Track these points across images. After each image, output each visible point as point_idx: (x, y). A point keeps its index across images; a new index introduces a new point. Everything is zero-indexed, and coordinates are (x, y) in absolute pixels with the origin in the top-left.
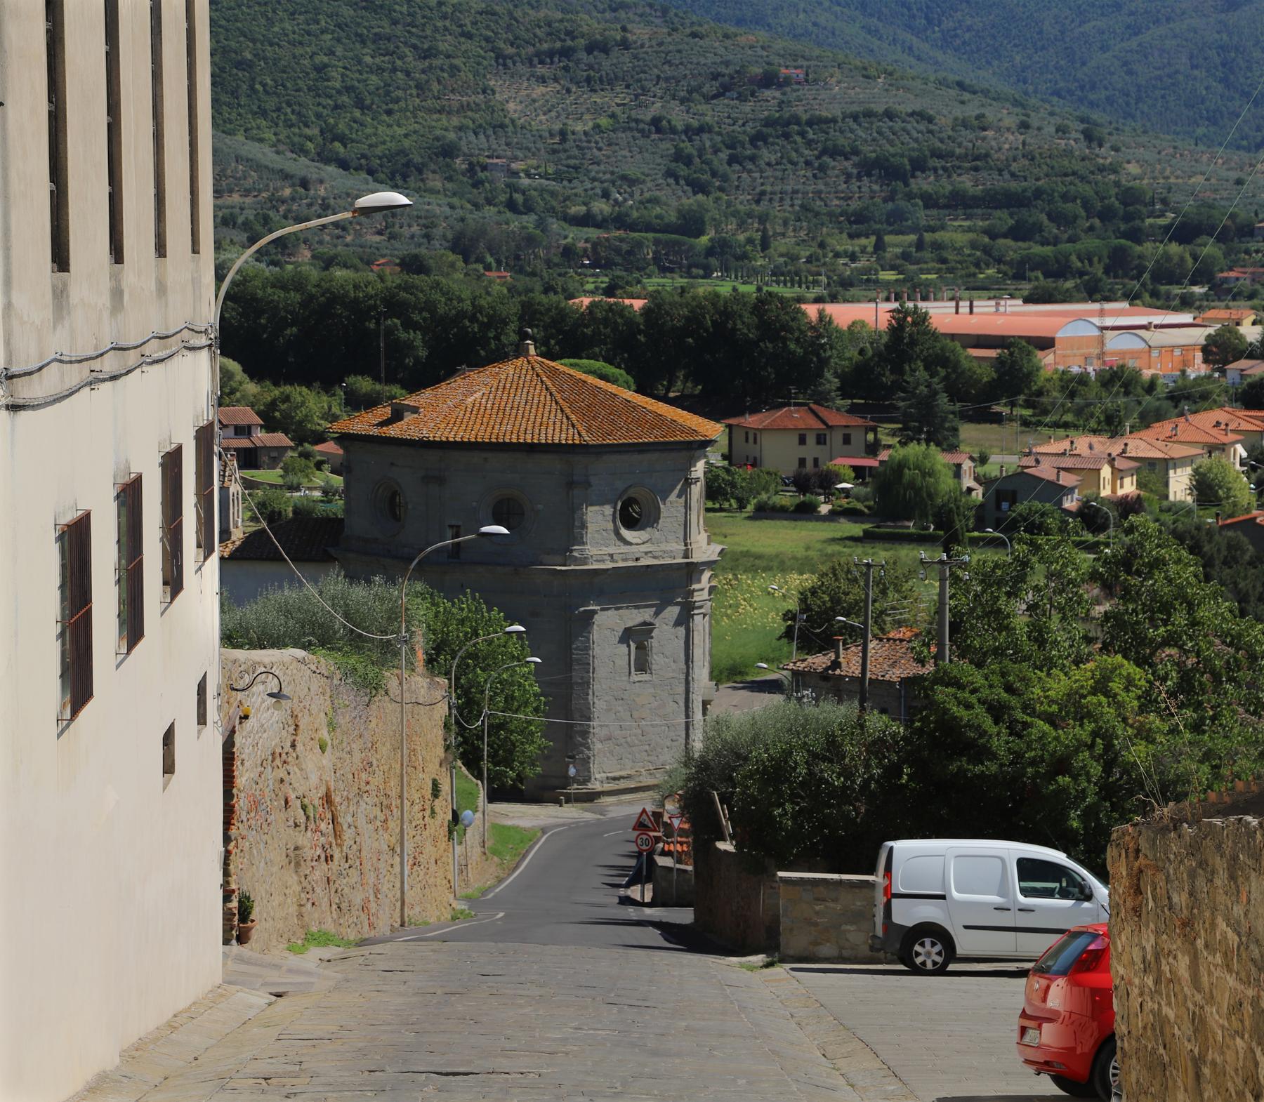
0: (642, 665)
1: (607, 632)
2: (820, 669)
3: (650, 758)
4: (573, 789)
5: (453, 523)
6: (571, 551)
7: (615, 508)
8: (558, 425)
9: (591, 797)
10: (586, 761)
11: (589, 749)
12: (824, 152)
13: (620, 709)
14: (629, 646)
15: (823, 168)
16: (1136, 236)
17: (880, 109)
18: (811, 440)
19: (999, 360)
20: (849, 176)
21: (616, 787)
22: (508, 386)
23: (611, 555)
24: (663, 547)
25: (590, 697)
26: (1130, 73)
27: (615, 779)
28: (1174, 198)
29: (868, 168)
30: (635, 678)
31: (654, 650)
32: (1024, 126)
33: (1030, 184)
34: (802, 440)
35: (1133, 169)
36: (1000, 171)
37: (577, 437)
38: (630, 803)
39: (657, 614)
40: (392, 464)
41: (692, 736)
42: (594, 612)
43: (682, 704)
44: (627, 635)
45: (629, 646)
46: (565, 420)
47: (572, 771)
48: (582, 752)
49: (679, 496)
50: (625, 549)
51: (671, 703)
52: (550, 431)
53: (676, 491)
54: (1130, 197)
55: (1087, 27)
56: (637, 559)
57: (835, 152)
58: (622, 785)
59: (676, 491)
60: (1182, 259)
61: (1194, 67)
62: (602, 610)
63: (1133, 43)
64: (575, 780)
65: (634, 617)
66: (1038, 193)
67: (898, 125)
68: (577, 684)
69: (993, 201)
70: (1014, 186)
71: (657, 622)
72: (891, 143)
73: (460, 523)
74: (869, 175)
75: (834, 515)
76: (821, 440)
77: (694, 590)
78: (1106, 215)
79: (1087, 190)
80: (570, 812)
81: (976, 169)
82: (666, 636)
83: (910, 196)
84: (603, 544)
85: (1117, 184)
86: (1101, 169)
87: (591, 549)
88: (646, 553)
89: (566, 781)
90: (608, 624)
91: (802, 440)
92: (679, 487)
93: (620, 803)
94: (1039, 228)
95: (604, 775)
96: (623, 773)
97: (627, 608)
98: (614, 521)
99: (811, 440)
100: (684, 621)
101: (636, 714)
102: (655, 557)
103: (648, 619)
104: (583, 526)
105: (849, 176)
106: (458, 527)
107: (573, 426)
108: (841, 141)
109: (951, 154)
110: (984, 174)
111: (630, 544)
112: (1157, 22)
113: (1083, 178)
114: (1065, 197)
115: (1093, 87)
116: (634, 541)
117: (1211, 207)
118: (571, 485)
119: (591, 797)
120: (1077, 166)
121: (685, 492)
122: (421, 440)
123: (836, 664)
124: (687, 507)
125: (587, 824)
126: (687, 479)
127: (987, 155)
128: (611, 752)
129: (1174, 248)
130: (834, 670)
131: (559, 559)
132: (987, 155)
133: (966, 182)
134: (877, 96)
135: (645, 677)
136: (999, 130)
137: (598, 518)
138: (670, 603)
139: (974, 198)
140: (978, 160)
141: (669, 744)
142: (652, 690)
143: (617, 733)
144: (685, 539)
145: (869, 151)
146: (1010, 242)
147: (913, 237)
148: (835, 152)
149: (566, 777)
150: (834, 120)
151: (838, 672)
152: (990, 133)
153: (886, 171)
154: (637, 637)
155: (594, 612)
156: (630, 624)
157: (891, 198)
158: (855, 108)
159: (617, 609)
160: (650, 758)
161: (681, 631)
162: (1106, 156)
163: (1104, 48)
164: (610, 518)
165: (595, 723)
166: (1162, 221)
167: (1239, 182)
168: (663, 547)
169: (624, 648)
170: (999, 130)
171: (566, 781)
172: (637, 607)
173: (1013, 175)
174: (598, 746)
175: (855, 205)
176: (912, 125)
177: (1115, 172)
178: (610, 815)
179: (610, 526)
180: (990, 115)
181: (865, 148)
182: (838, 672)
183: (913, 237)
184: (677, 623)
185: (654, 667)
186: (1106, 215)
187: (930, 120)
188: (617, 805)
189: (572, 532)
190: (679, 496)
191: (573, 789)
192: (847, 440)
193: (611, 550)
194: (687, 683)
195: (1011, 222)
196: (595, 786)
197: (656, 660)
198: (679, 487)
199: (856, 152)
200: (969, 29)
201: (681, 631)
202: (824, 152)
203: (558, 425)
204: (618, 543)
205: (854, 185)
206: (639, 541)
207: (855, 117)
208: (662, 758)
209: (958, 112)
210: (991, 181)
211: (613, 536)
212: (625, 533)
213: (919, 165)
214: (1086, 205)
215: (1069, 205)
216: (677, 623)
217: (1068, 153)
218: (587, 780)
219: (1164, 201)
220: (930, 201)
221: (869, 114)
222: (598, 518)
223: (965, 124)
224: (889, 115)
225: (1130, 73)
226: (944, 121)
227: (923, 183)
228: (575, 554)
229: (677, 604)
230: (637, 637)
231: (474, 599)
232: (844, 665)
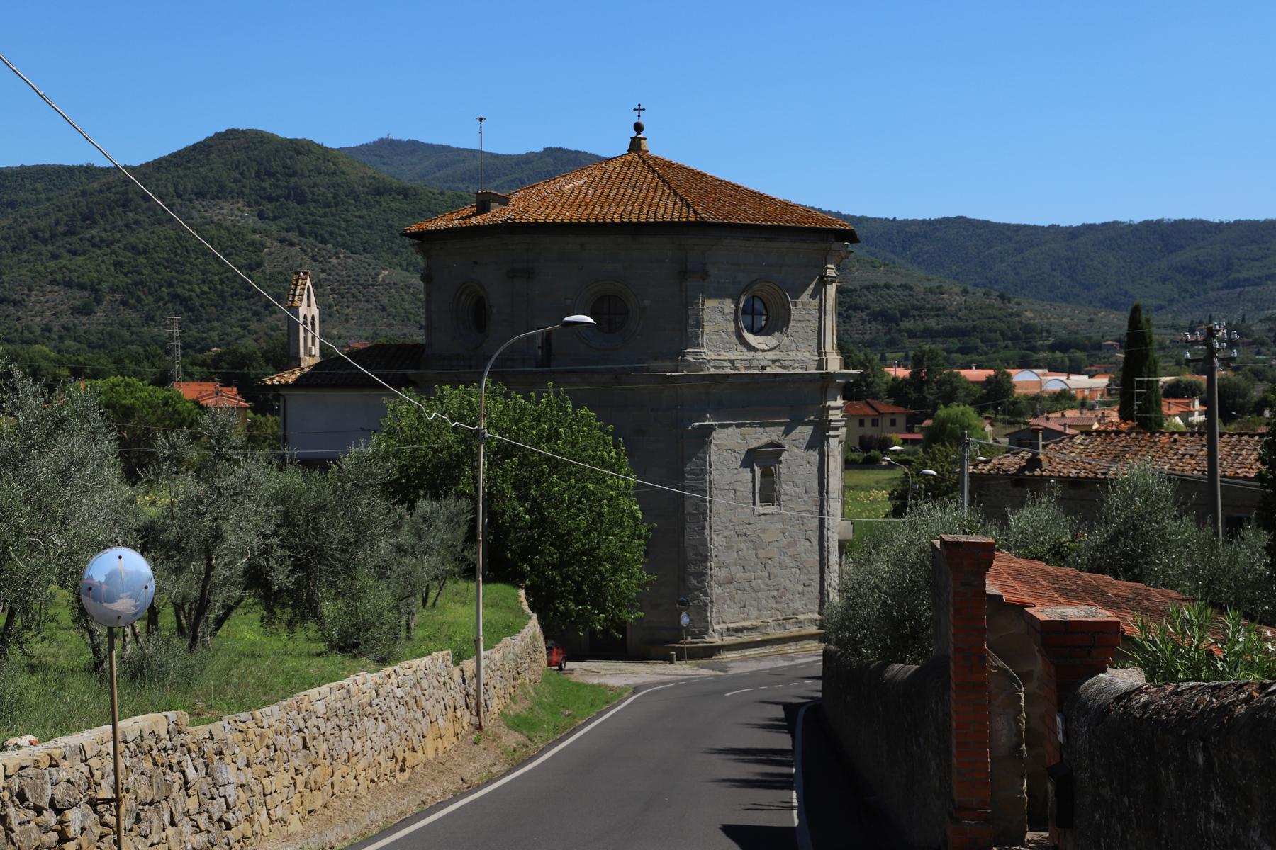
0: (769, 494)
1: (728, 454)
2: (1012, 471)
3: (779, 606)
4: (688, 642)
6: (684, 355)
7: (737, 306)
8: (670, 206)
9: (709, 652)
10: (703, 608)
11: (706, 594)
12: (850, 308)
13: (743, 546)
14: (753, 471)
15: (849, 317)
16: (1034, 349)
17: (882, 283)
18: (868, 423)
19: (989, 381)
20: (864, 321)
21: (739, 640)
22: (614, 176)
23: (732, 362)
24: (793, 355)
25: (707, 532)
26: (1017, 274)
27: (737, 630)
28: (1053, 329)
29: (875, 317)
30: (760, 509)
31: (783, 478)
32: (965, 292)
33: (970, 323)
34: (862, 424)
35: (1029, 314)
36: (952, 317)
37: (692, 215)
38: (756, 658)
39: (787, 433)
40: (475, 263)
41: (828, 580)
42: (712, 428)
43: (815, 543)
44: (751, 458)
45: (753, 471)
46: (678, 201)
47: (685, 620)
48: (698, 598)
49: (813, 296)
50: (748, 355)
51: (803, 541)
52: (661, 212)
53: (809, 291)
54: (1029, 329)
55: (992, 250)
56: (763, 368)
57: (856, 308)
58: (746, 637)
59: (809, 291)
60: (1063, 361)
61: (1054, 270)
62: (721, 426)
63: (1019, 258)
64: (688, 631)
65: (760, 436)
66: (975, 328)
67: (892, 292)
68: (691, 514)
69: (948, 333)
70: (961, 325)
71: (785, 443)
72: (888, 302)
74: (876, 320)
75: (890, 466)
76: (875, 423)
77: (830, 408)
78: (1015, 338)
79: (1004, 326)
80: (683, 669)
81: (938, 316)
82: (797, 461)
83: (900, 331)
84: (721, 344)
85: (1020, 322)
86: (1010, 315)
87: (708, 353)
88: (774, 361)
89: (678, 633)
90: (729, 443)
91: (862, 424)
92: (812, 286)
93: (744, 659)
94: (977, 348)
95: (724, 626)
96: (747, 624)
97: (751, 425)
98: (736, 321)
99: (868, 423)
100: (818, 442)
101: (762, 553)
102: (783, 367)
103: (774, 437)
104: (699, 324)
105: (864, 321)
107: (688, 206)
108: (859, 301)
109: (924, 308)
110: (942, 318)
111: (755, 350)
112: (1032, 246)
113: (1000, 320)
114: (990, 330)
115: (997, 282)
116: (759, 347)
117: (1076, 333)
118: (684, 273)
119: (709, 652)
120: (997, 313)
121: (819, 293)
122: (505, 223)
123: (1034, 463)
124: (822, 310)
125: (702, 681)
126: (821, 277)
127: (944, 308)
128: (732, 599)
129: (1058, 354)
130: (1032, 470)
131: (668, 364)
132: (944, 308)
133: (932, 323)
134: (880, 276)
136: (950, 294)
137: (717, 315)
138: (802, 422)
139: (937, 332)
140: (939, 311)
141: (800, 588)
142: (780, 526)
143: (740, 575)
144: (819, 348)
145: (875, 307)
146: (959, 355)
147: (902, 354)
148: (856, 308)
149: (678, 627)
150: (855, 290)
151: (1037, 472)
152: (945, 296)
153: (885, 317)
154: (763, 461)
155: (712, 428)
156: (754, 445)
157: (889, 332)
158: (867, 283)
159: (739, 426)
161: (814, 455)
162: (1012, 307)
163: (1002, 262)
164: (731, 317)
165: (713, 563)
166: (1047, 343)
167: (1091, 320)
168: (793, 355)
169: (746, 474)
170: (950, 294)
171: (678, 633)
172: (761, 425)
173: (959, 319)
175: (867, 337)
176: (900, 292)
177: (1018, 316)
178: (732, 672)
179: (732, 327)
180: (946, 286)
181: (873, 305)
182: (1037, 472)
183: (902, 354)
184: (810, 446)
185: (783, 498)
186: (1015, 338)
187: (911, 289)
188: (740, 661)
189: (686, 330)
190: (813, 296)
191: (688, 642)
192: (893, 423)
193: (731, 356)
194: (822, 507)
195: (959, 345)
196: (716, 640)
197: (786, 489)
198: (812, 286)
199: (867, 307)
200: (926, 252)
201: (814, 455)
202: (850, 308)
203: (670, 206)
204: (741, 348)
205: (867, 326)
206: (765, 347)
207: (867, 288)
208: (794, 606)
209: (927, 285)
210: (947, 322)
212: (749, 337)
213: (905, 314)
214: (1002, 334)
215: (993, 335)
216: (810, 446)
217: (991, 306)
218: (704, 632)
219: (1048, 331)
220: (911, 334)
221: (876, 287)
222: (717, 315)
223: (931, 291)
224: (887, 286)
225: (1017, 274)
226: (919, 289)
227: (907, 324)
228: (689, 358)
229: (809, 423)
230: (763, 461)
231: (557, 394)
232: (1045, 464)
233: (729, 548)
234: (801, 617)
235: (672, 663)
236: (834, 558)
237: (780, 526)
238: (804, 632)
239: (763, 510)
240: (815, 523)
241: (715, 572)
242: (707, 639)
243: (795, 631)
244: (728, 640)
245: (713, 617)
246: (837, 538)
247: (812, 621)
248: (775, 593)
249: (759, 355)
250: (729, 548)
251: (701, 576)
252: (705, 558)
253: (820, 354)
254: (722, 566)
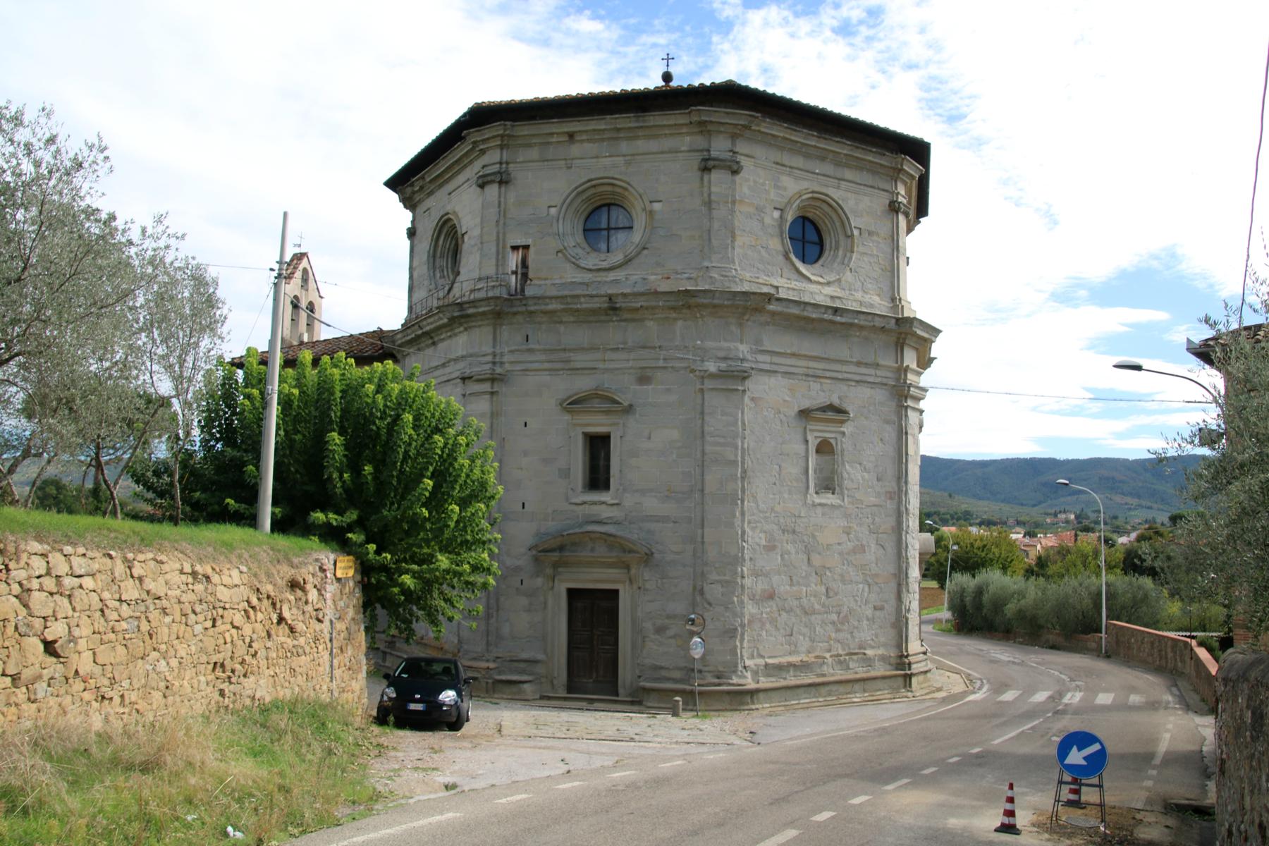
3: (841, 636)
5: (519, 241)
21: (782, 683)
25: (738, 522)
58: (792, 681)
73: (529, 242)
95: (761, 662)
96: (794, 659)
106: (526, 247)
128: (773, 621)
135: (828, 498)
142: (843, 523)
143: (783, 588)
160: (841, 636)
168: (859, 295)
174: (750, 609)
211: (781, 258)
233: (770, 548)
234: (870, 652)
235: (675, 714)
236: (915, 572)
237: (843, 523)
238: (873, 674)
239: (817, 500)
240: (891, 522)
241: (748, 582)
242: (735, 680)
243: (861, 672)
244: (765, 683)
245: (744, 647)
246: (917, 546)
247: (883, 658)
248: (834, 617)
249: (813, 287)
250: (770, 548)
251: (730, 585)
252: (738, 560)
253: (893, 300)
254: (756, 574)
